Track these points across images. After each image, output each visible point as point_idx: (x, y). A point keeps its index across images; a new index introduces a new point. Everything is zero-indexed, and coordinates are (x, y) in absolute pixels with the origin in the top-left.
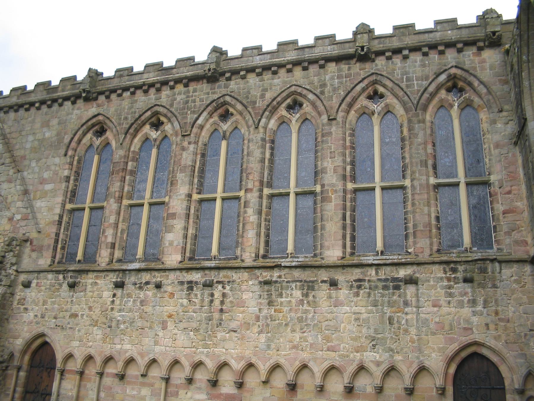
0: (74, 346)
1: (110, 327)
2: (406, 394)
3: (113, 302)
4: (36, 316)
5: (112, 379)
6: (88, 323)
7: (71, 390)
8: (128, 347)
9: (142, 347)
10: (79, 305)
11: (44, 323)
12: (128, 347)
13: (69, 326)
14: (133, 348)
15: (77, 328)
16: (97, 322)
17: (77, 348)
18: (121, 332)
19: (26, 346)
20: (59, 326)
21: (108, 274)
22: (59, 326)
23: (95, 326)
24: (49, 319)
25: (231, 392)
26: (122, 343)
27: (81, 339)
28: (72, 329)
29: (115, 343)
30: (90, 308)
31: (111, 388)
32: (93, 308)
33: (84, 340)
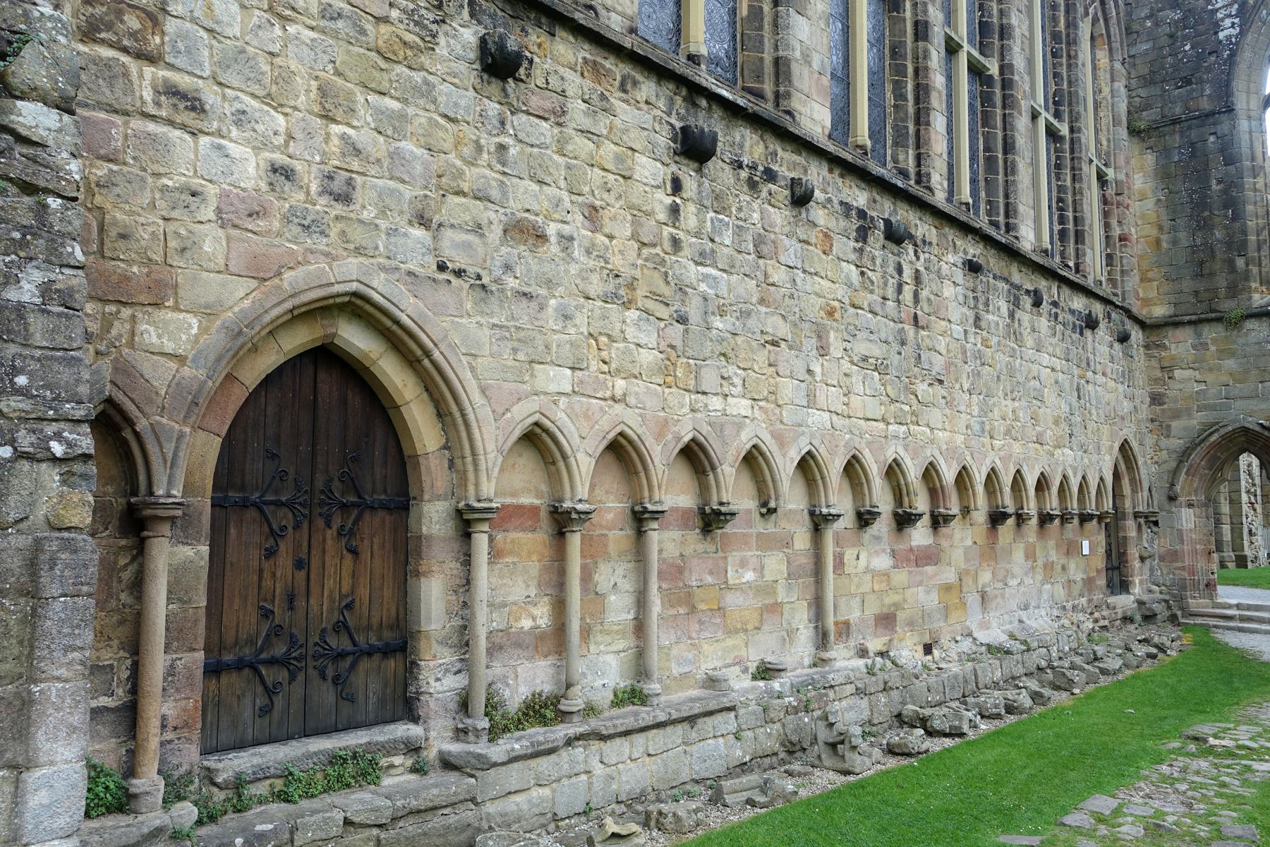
0: (552, 388)
1: (682, 320)
2: (96, 712)
3: (675, 210)
4: (281, 173)
5: (676, 534)
6: (596, 285)
7: (528, 600)
8: (740, 406)
9: (777, 411)
10: (541, 182)
11: (358, 235)
12: (740, 406)
13: (511, 283)
14: (757, 413)
15: (553, 302)
16: (631, 286)
17: (563, 399)
18: (719, 348)
19: (938, 485)
20: (459, 273)
21: (639, 77)
22: (459, 273)
23: (627, 305)
24: (383, 213)
25: (925, 543)
26: (726, 390)
27: (580, 360)
28: (534, 304)
29: (704, 388)
30: (593, 214)
31: (680, 570)
32: (606, 214)
33: (593, 368)
